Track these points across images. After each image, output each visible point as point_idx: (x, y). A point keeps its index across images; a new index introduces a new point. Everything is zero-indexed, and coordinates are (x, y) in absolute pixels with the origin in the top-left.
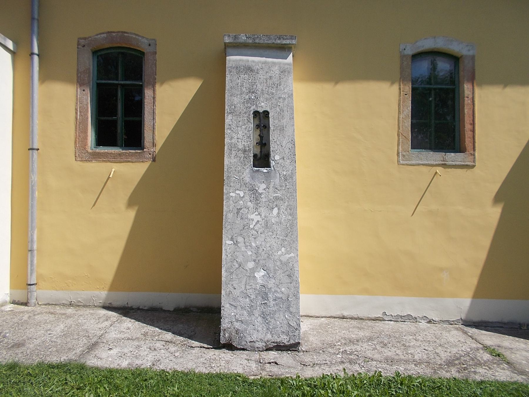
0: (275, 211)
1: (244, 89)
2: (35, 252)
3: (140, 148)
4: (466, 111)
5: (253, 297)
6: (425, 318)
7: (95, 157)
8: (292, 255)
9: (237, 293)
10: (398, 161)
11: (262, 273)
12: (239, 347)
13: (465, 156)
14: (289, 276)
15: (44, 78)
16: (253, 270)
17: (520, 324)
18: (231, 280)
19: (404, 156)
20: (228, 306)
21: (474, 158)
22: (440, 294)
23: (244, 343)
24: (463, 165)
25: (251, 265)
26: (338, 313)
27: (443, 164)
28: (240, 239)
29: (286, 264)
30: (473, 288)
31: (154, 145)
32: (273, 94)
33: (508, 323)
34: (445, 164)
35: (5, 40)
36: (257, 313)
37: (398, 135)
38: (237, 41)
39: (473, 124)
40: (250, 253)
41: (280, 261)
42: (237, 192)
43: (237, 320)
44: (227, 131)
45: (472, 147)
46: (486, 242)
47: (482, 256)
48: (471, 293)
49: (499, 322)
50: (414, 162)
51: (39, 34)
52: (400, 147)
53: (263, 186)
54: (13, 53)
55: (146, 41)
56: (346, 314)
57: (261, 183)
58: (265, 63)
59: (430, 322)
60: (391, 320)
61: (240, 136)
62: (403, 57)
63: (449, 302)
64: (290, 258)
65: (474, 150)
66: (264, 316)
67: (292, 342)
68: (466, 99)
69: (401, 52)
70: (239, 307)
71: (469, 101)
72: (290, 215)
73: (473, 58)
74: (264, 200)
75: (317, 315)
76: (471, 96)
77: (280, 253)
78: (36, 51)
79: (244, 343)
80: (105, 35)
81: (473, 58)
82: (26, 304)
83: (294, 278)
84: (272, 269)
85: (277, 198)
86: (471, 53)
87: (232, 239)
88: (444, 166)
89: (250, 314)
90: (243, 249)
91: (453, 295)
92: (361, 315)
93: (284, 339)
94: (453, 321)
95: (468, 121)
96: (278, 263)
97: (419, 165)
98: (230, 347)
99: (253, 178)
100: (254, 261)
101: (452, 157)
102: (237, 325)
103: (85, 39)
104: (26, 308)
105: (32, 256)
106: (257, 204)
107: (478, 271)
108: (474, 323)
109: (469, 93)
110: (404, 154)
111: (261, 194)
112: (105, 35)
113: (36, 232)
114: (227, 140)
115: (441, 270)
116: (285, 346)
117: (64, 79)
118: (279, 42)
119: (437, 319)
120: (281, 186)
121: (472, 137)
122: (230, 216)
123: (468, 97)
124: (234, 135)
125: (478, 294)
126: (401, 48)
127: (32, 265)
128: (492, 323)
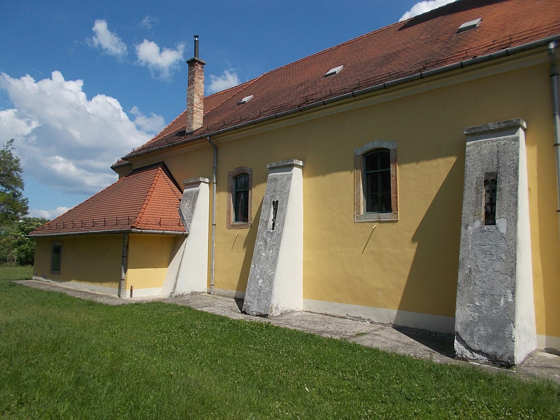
0: (272, 251)
1: (272, 190)
2: (213, 270)
3: (61, 248)
4: (391, 185)
5: (256, 291)
6: (369, 320)
7: (233, 227)
8: (273, 273)
9: (251, 289)
10: (354, 221)
11: (262, 280)
12: (248, 313)
13: (392, 214)
14: (270, 283)
15: (218, 191)
16: (259, 279)
17: (430, 332)
18: (250, 283)
19: (357, 217)
20: (247, 295)
21: (397, 216)
22: (376, 305)
23: (249, 312)
24: (390, 221)
25: (258, 277)
26: (324, 312)
27: (378, 221)
28: (257, 265)
29: (270, 277)
30: (398, 303)
31: (251, 220)
32: (282, 191)
33: (422, 330)
34: (380, 221)
35: (204, 179)
36: (256, 299)
37: (354, 205)
38: (271, 166)
39: (396, 193)
40: (259, 271)
41: (269, 275)
42: (260, 242)
43: (249, 301)
44: (262, 213)
45: (396, 208)
46: (406, 271)
47: (404, 281)
48: (397, 307)
49: (416, 329)
50: (362, 221)
51: (216, 174)
52: (355, 212)
53: (269, 239)
54: (209, 183)
55: (249, 169)
56: (328, 313)
57: (269, 238)
58: (282, 175)
59: (371, 323)
60: (350, 319)
61: (266, 215)
62: (356, 157)
63: (383, 311)
64: (272, 274)
65: (397, 210)
66: (258, 300)
67: (265, 313)
68: (391, 177)
69: (355, 154)
70: (251, 296)
71: (394, 179)
72: (276, 253)
73: (395, 150)
74: (268, 246)
75: (315, 312)
76: (394, 175)
77: (269, 271)
78: (215, 182)
79: (249, 312)
80: (236, 170)
81: (395, 150)
82: (210, 294)
83: (272, 284)
84: (265, 279)
85: (273, 245)
86: (394, 147)
87: (254, 265)
88: (379, 222)
89: (254, 299)
90: (257, 269)
91: (385, 307)
92: (335, 314)
93: (263, 312)
94: (386, 324)
95: (393, 192)
96: (268, 276)
97: (365, 222)
98: (245, 313)
99: (266, 235)
100: (260, 275)
101: (385, 216)
102: (249, 303)
103: (230, 172)
104: (210, 295)
105: (212, 273)
106: (266, 248)
107: (401, 292)
108: (399, 327)
109: (394, 173)
110: (358, 216)
111: (268, 243)
112: (236, 170)
113: (214, 262)
114: (261, 217)
115: (378, 289)
116: (263, 315)
117: (223, 190)
118: (287, 164)
119: (376, 321)
120: (276, 239)
121: (395, 201)
122: (255, 253)
123: (393, 176)
124: (264, 214)
125: (401, 308)
126: (355, 152)
127: (212, 276)
128: (411, 328)
